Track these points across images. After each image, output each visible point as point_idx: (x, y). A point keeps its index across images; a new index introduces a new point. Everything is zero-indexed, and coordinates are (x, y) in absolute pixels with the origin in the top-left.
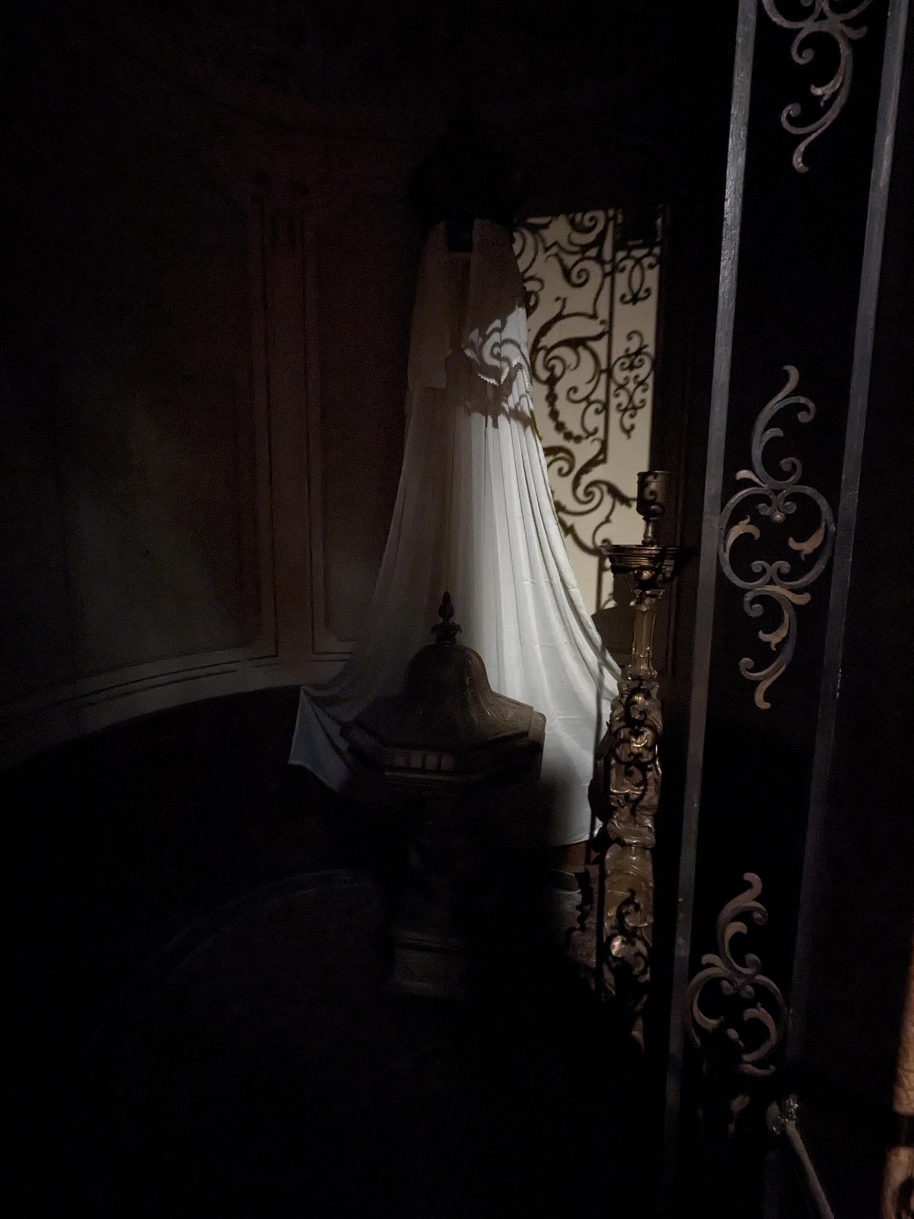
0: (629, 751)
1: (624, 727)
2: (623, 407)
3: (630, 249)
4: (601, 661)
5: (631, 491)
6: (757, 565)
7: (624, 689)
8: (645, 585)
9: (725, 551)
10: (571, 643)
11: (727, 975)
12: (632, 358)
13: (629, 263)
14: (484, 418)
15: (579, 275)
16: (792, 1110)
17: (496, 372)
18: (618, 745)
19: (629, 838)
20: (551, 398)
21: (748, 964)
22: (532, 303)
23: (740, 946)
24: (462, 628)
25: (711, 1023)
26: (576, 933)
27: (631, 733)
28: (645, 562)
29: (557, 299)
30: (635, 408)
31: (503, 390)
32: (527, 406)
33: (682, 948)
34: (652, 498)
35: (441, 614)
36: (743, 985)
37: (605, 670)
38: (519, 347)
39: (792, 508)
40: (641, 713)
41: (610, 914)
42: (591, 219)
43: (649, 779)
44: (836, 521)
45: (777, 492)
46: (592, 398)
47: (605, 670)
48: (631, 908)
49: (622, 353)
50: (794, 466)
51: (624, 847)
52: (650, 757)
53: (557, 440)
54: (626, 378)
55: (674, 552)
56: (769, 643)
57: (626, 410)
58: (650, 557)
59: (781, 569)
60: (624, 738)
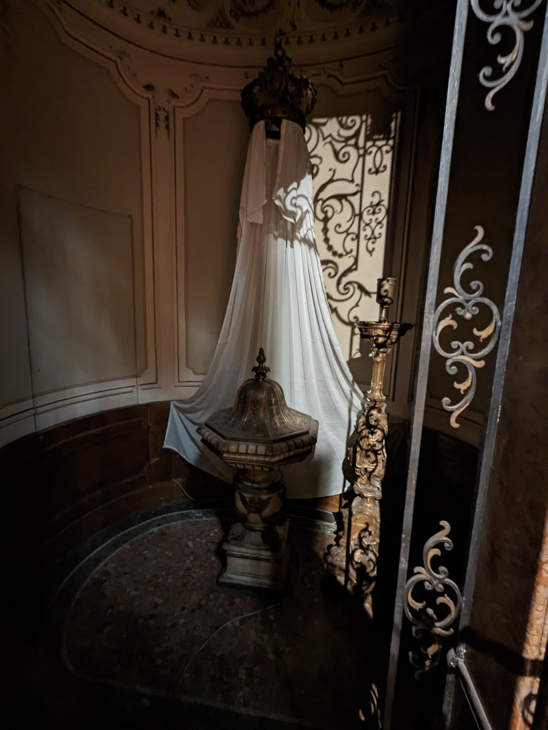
0: (368, 443)
1: (364, 429)
2: (368, 237)
3: (375, 141)
4: (351, 389)
5: (372, 287)
6: (455, 344)
7: (366, 407)
8: (379, 346)
9: (436, 335)
10: (335, 379)
11: (428, 579)
12: (375, 207)
13: (374, 149)
14: (285, 242)
15: (344, 156)
16: (462, 653)
17: (293, 215)
18: (361, 439)
19: (366, 493)
20: (325, 230)
21: (440, 573)
22: (315, 171)
23: (436, 563)
24: (270, 369)
25: (418, 606)
26: (334, 548)
27: (369, 433)
28: (380, 332)
29: (330, 170)
30: (375, 238)
31: (297, 226)
32: (311, 236)
33: (404, 564)
34: (385, 294)
35: (258, 361)
36: (437, 584)
37: (354, 394)
38: (307, 199)
39: (477, 311)
40: (376, 421)
41: (354, 537)
42: (352, 121)
43: (379, 459)
44: (501, 319)
45: (467, 301)
46: (350, 231)
47: (354, 394)
48: (367, 534)
49: (369, 204)
50: (478, 287)
51: (363, 499)
52: (380, 447)
53: (329, 256)
54: (371, 220)
55: (398, 327)
56: (460, 390)
57: (370, 239)
58: (383, 330)
59: (468, 347)
60: (365, 435)
